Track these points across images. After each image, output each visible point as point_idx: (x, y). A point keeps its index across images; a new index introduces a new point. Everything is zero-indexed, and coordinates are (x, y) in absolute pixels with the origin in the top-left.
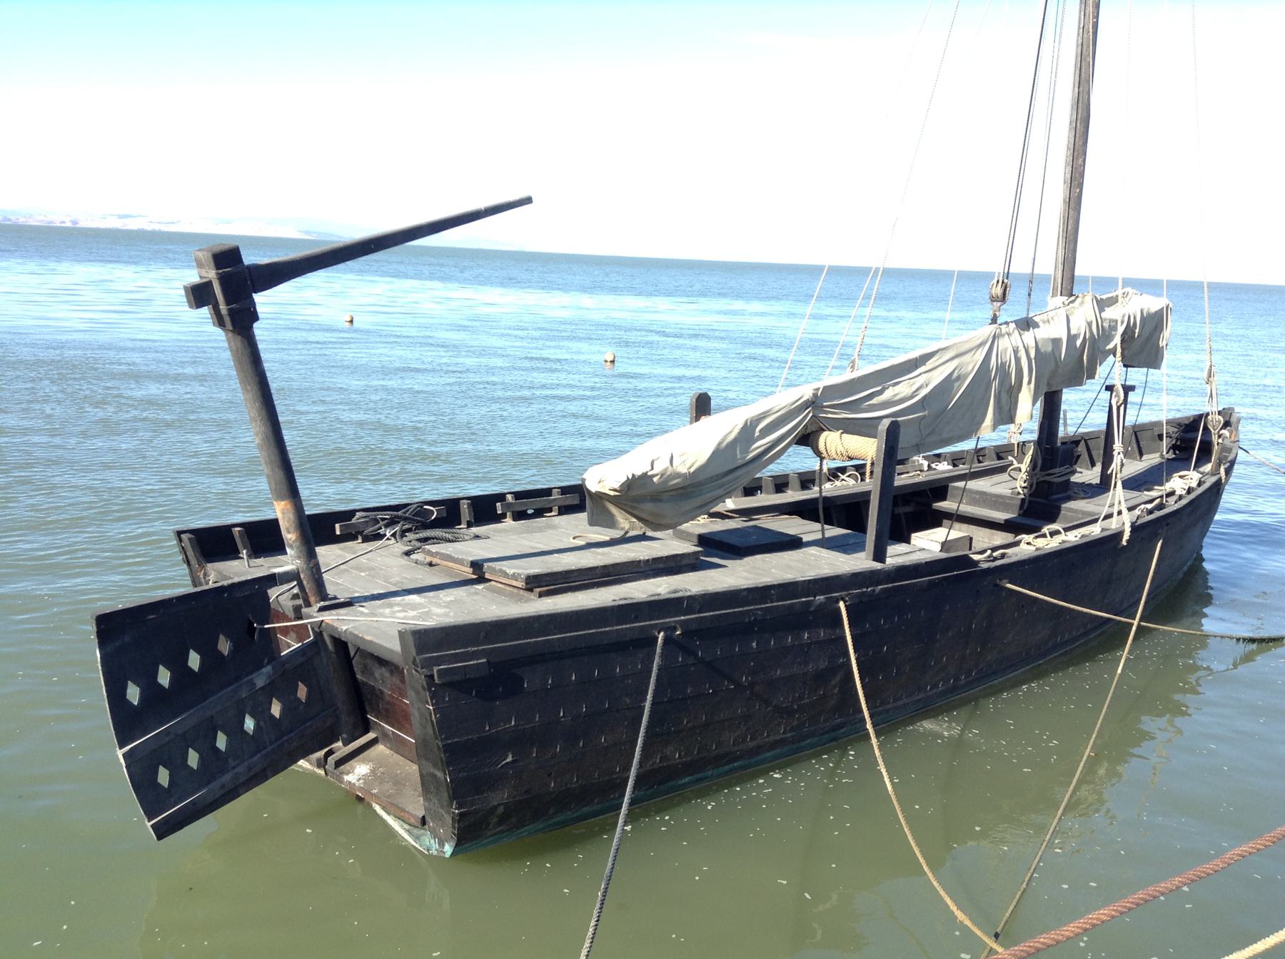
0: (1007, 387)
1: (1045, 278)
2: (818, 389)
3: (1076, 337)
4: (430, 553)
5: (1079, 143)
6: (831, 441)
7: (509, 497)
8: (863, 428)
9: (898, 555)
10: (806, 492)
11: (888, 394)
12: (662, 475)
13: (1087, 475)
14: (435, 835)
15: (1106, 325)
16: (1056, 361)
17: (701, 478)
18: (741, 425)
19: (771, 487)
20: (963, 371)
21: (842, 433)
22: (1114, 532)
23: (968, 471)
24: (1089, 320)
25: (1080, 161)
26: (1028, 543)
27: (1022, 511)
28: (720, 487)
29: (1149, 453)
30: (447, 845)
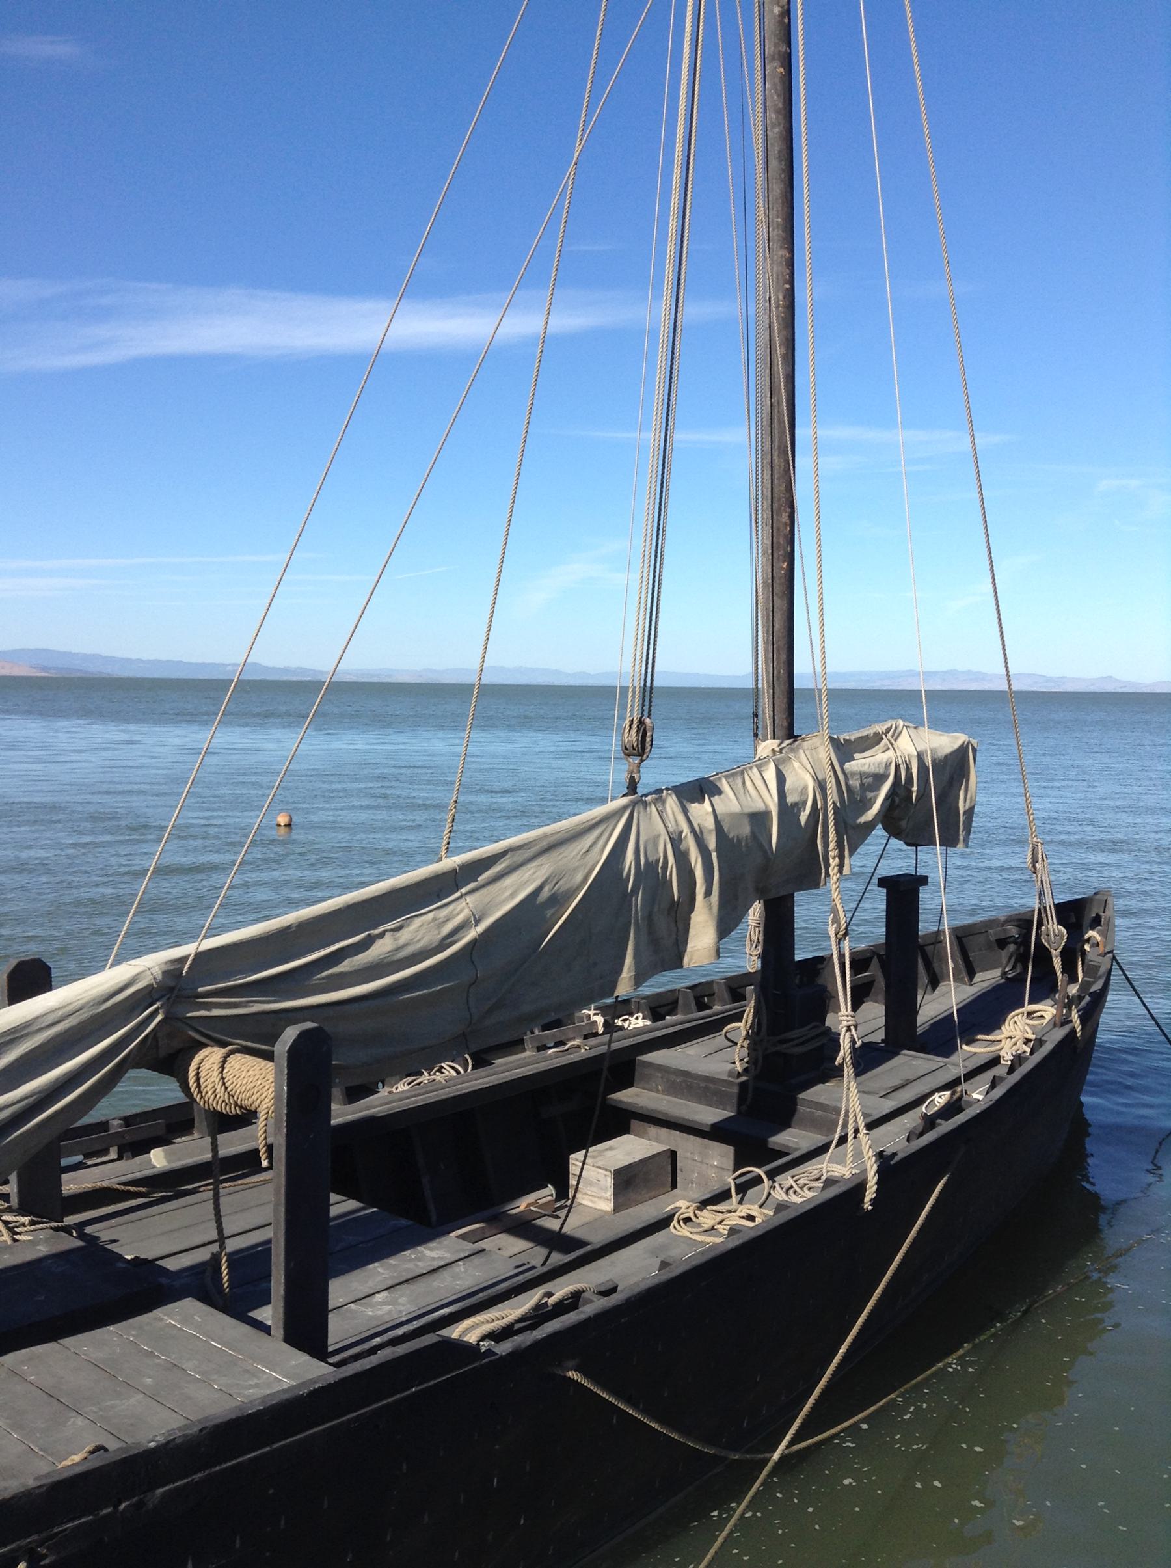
3: (799, 806)
11: (380, 949)
15: (855, 783)
16: (765, 852)
20: (563, 886)
22: (851, 1185)
25: (785, 517)
27: (744, 1108)
29: (984, 970)
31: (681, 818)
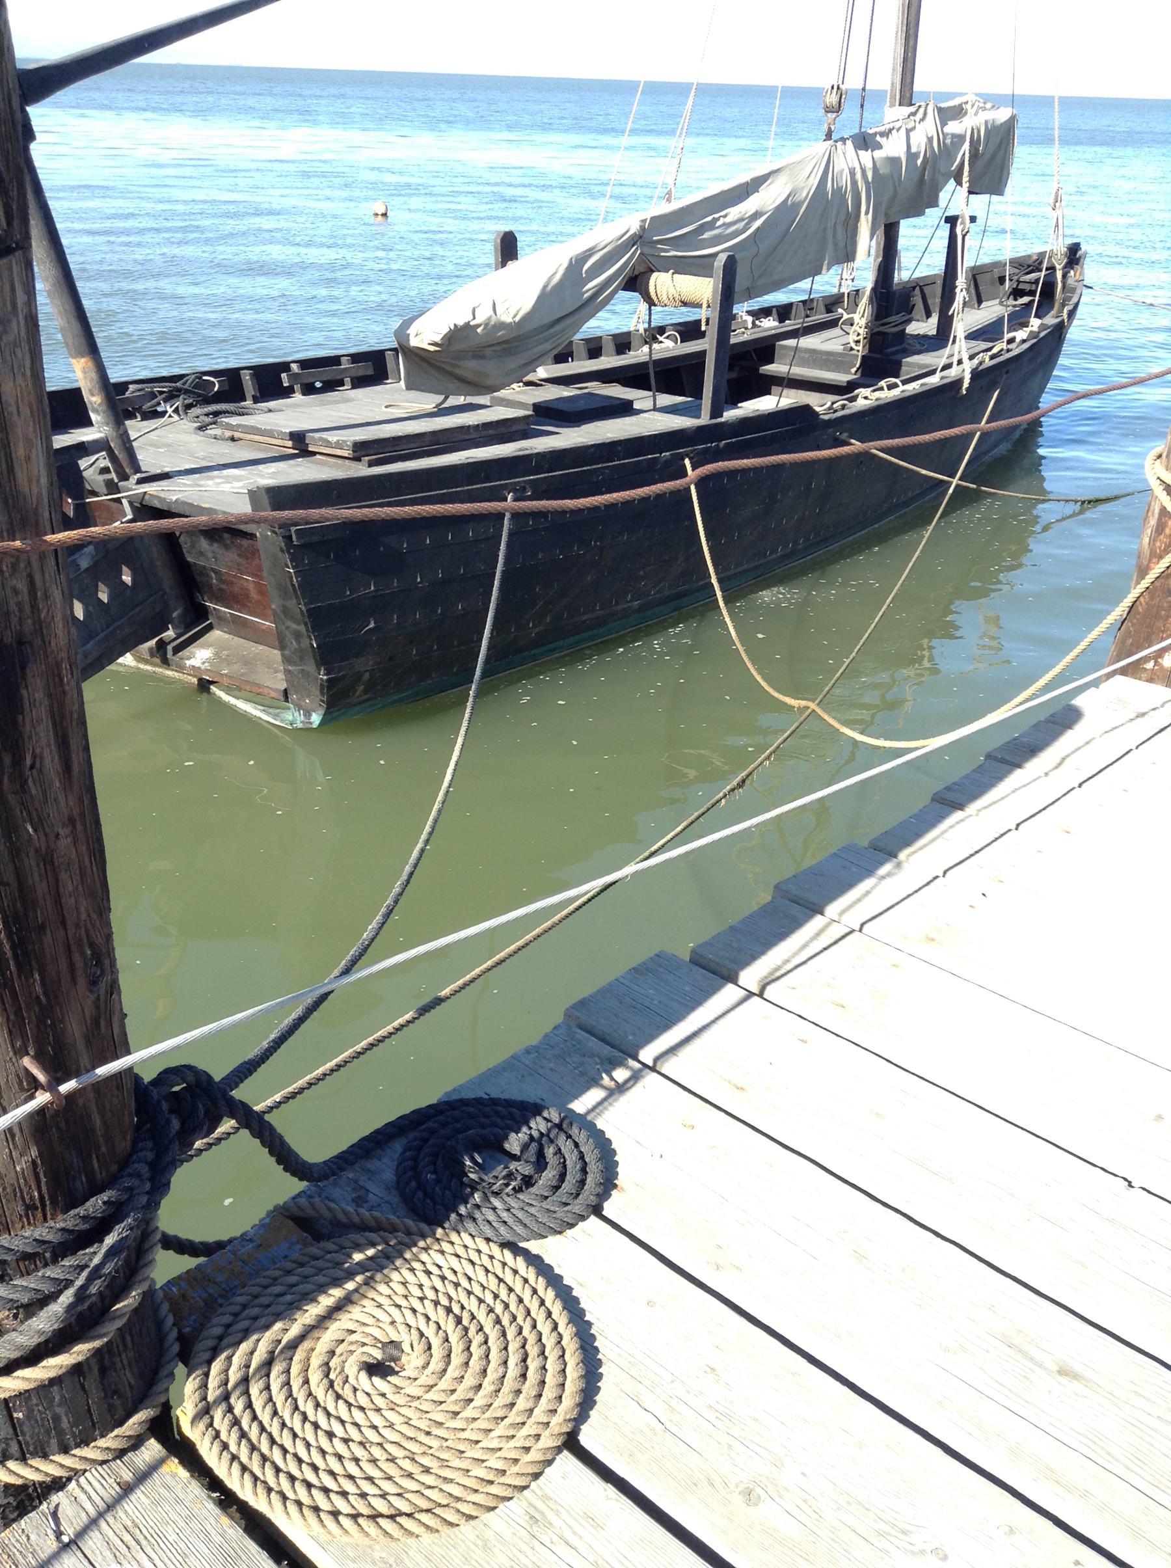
0: (843, 216)
2: (644, 221)
3: (917, 155)
4: (229, 427)
6: (662, 283)
7: (295, 367)
8: (698, 267)
9: (731, 415)
10: (623, 356)
12: (486, 325)
13: (923, 327)
14: (299, 707)
17: (529, 327)
18: (565, 265)
19: (584, 353)
21: (673, 273)
23: (800, 326)
26: (866, 398)
28: (546, 341)
30: (314, 714)
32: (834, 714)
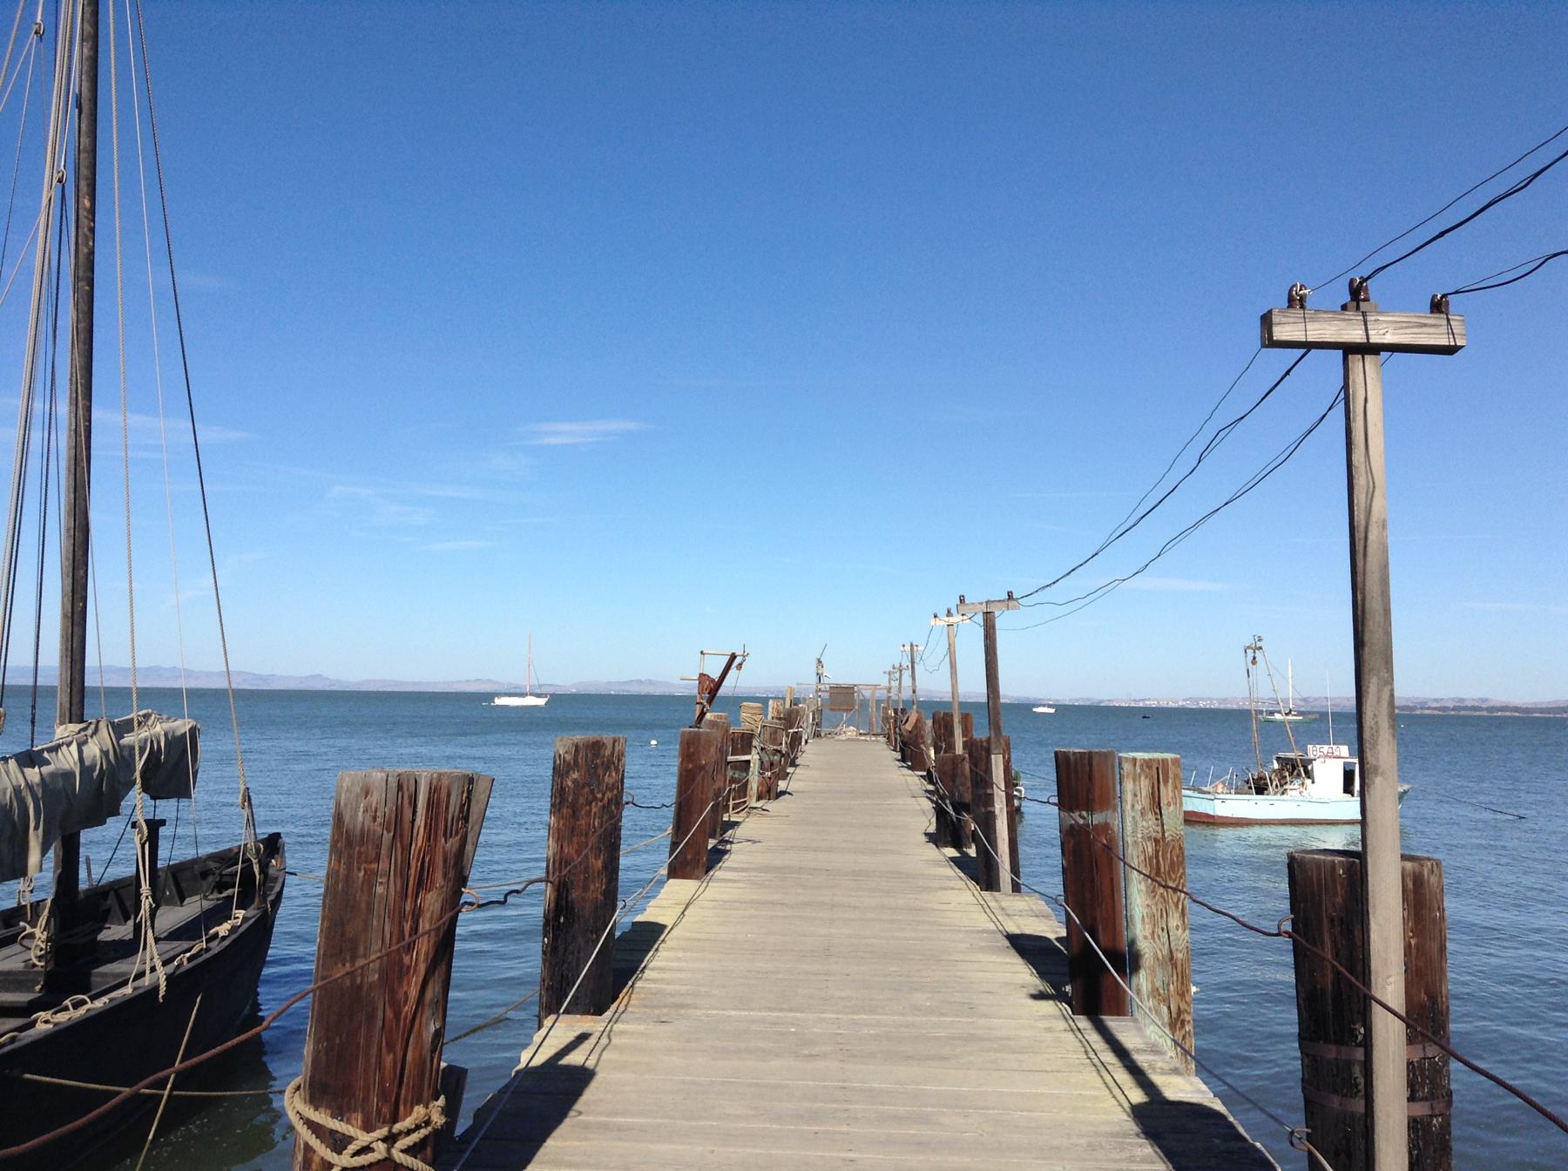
1: (51, 691)
3: (92, 768)
5: (79, 553)
24: (105, 749)
25: (82, 572)
26: (47, 1022)
31: (20, 776)
32: (582, 965)
